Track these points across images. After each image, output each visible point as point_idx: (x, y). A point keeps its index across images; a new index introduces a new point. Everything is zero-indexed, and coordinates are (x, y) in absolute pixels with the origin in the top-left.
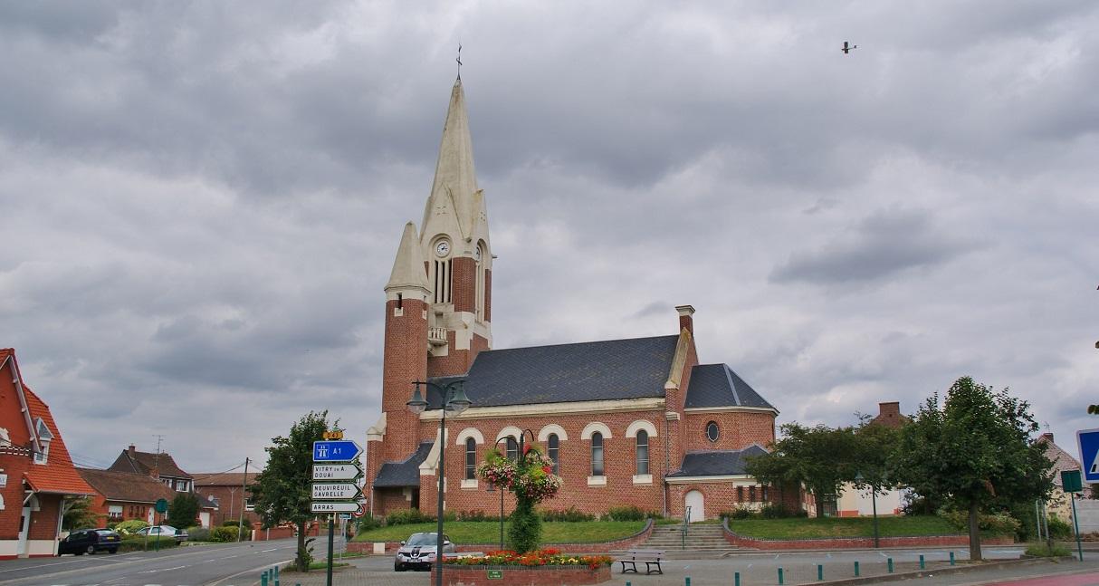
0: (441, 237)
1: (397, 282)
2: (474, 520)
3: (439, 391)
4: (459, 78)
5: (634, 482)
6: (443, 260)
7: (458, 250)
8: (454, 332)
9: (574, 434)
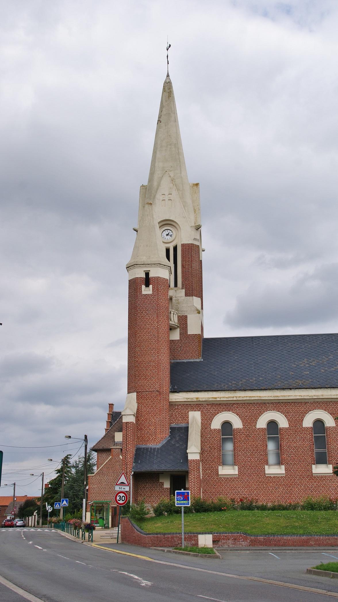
0: (167, 223)
1: (144, 259)
2: (243, 508)
3: (181, 377)
4: (168, 76)
5: (314, 472)
6: (167, 245)
7: (185, 237)
8: (186, 317)
9: (250, 421)
